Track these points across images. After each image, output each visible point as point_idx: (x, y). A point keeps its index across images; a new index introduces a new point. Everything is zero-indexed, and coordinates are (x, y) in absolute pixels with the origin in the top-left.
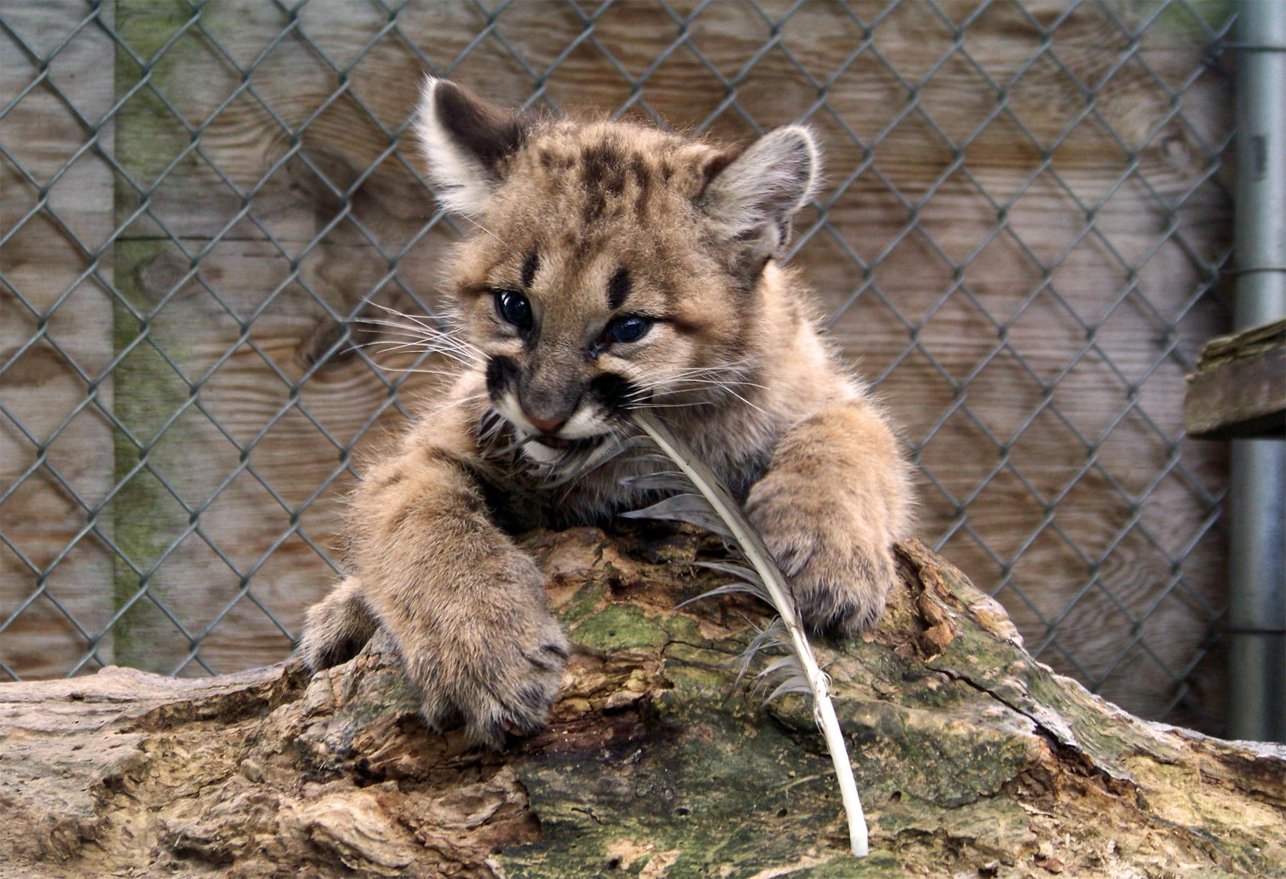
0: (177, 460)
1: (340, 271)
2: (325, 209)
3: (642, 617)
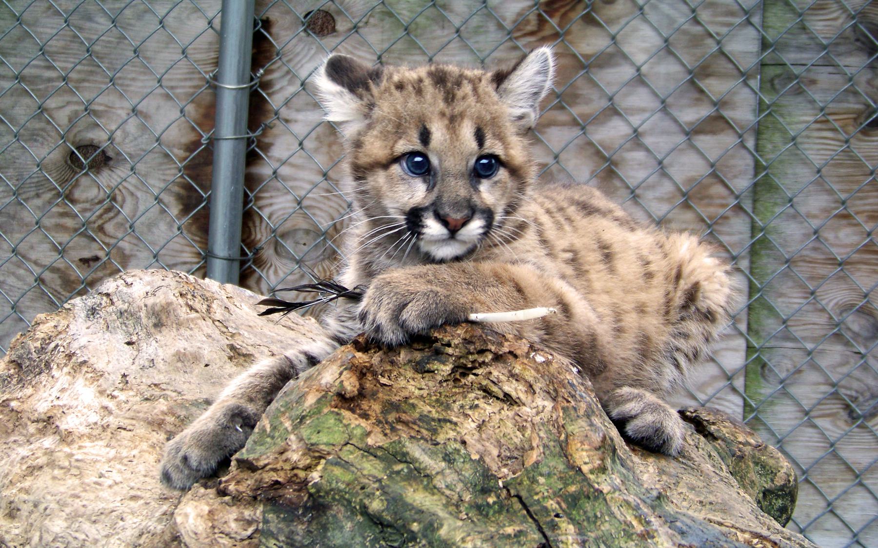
0: (789, 171)
3: (341, 422)
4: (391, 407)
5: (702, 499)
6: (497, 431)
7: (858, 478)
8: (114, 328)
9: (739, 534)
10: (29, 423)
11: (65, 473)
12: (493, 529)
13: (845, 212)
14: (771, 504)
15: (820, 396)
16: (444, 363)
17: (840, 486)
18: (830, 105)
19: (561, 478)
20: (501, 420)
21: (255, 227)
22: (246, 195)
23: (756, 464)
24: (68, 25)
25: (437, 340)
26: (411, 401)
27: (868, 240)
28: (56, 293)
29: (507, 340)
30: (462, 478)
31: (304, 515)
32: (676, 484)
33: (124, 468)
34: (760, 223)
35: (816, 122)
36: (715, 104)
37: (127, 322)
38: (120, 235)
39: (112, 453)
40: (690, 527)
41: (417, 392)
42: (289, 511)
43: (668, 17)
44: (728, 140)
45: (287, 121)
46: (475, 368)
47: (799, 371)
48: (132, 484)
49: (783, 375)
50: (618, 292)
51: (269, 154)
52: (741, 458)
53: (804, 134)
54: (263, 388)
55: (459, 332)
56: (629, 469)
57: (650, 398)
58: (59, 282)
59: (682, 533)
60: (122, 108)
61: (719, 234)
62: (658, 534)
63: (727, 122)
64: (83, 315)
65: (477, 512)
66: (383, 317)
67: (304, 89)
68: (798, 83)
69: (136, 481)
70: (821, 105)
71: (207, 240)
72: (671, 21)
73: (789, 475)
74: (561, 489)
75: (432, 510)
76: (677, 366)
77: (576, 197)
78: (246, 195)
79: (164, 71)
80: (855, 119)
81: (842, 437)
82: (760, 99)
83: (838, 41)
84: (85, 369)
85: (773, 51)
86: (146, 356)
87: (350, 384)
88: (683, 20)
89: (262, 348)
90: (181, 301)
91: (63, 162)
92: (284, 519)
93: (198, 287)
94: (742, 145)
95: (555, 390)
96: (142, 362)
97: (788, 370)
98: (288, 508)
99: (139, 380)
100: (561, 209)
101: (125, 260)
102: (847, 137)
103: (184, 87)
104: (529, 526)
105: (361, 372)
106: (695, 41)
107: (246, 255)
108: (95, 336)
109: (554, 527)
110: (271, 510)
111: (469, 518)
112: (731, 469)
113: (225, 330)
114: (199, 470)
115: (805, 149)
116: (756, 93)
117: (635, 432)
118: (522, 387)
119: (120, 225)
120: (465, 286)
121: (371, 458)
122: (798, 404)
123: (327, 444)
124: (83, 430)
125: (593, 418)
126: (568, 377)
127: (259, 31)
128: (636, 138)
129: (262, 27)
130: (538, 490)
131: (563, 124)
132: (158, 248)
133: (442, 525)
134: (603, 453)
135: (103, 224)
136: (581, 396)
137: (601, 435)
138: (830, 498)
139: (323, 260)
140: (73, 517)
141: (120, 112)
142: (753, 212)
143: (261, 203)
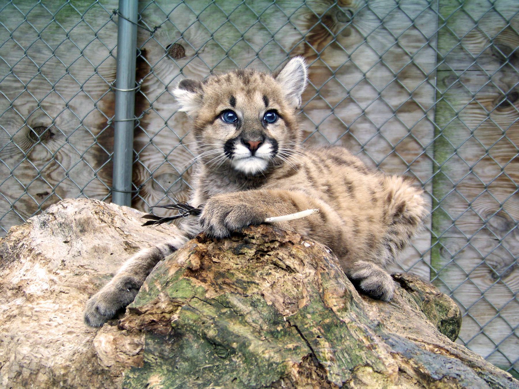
0: (455, 133)
1: (507, 80)
2: (502, 60)
3: (190, 284)
4: (219, 275)
5: (404, 326)
6: (282, 288)
7: (498, 313)
8: (57, 234)
9: (426, 345)
10: (8, 290)
11: (29, 319)
12: (280, 346)
13: (488, 157)
14: (446, 328)
15: (475, 266)
16: (250, 249)
17: (487, 318)
18: (478, 94)
19: (320, 315)
20: (285, 281)
21: (140, 173)
22: (134, 154)
23: (437, 305)
24: (26, 56)
25: (246, 235)
26: (231, 271)
27: (502, 173)
28: (23, 214)
29: (287, 234)
30: (262, 316)
31: (169, 340)
32: (389, 317)
33: (64, 315)
34: (438, 164)
35: (470, 104)
36: (410, 95)
37: (64, 230)
38: (60, 179)
39: (57, 307)
40: (397, 342)
41: (235, 266)
42: (160, 338)
43: (381, 43)
44: (418, 115)
45: (157, 110)
46: (269, 251)
47: (462, 251)
48: (69, 325)
49: (453, 254)
50: (357, 210)
51: (148, 130)
52: (428, 302)
53: (463, 111)
54: (144, 265)
55: (259, 230)
56: (360, 309)
57: (376, 267)
58: (25, 208)
59: (393, 346)
60: (60, 104)
61: (414, 171)
62: (378, 347)
63: (418, 105)
64: (38, 226)
65: (271, 336)
66: (214, 221)
67: (167, 91)
68: (459, 81)
69: (71, 322)
70: (473, 94)
71: (112, 181)
72: (383, 46)
73: (456, 311)
74: (320, 321)
75: (245, 335)
76: (390, 250)
77: (333, 154)
78: (134, 154)
79: (84, 82)
80: (493, 102)
81: (488, 289)
82: (437, 91)
83: (482, 56)
84: (40, 258)
85: (444, 62)
86: (76, 249)
87: (195, 262)
88: (389, 45)
89: (144, 243)
90: (96, 216)
91: (26, 137)
92: (158, 343)
93: (106, 208)
94: (427, 118)
95: (316, 263)
96: (73, 253)
97: (456, 251)
98: (160, 336)
99: (72, 264)
100: (323, 161)
101: (64, 194)
102: (488, 112)
103: (96, 91)
104: (302, 344)
105: (201, 255)
106: (398, 58)
107: (135, 189)
108: (45, 238)
109: (317, 343)
110: (150, 337)
111: (266, 339)
112: (422, 309)
113: (122, 233)
114: (105, 315)
115: (464, 120)
116: (434, 88)
117: (366, 287)
118: (296, 262)
119: (60, 173)
120: (262, 202)
121: (208, 305)
122: (462, 271)
123: (182, 298)
124: (40, 293)
125: (339, 279)
126: (324, 255)
127: (140, 57)
128: (364, 116)
129: (142, 54)
130: (307, 322)
131: (321, 108)
132: (83, 187)
133: (250, 344)
134: (345, 299)
135: (50, 173)
136: (332, 266)
137: (344, 289)
138: (481, 325)
139: (181, 191)
140: (35, 345)
141: (58, 106)
142: (434, 158)
143: (144, 158)
